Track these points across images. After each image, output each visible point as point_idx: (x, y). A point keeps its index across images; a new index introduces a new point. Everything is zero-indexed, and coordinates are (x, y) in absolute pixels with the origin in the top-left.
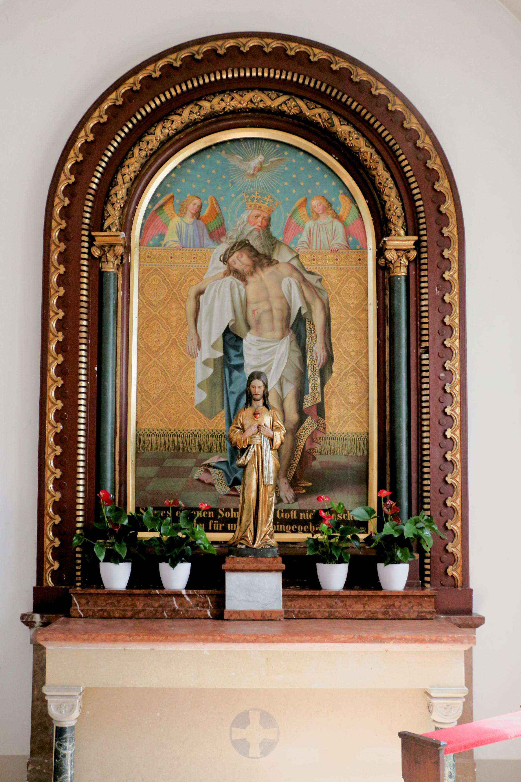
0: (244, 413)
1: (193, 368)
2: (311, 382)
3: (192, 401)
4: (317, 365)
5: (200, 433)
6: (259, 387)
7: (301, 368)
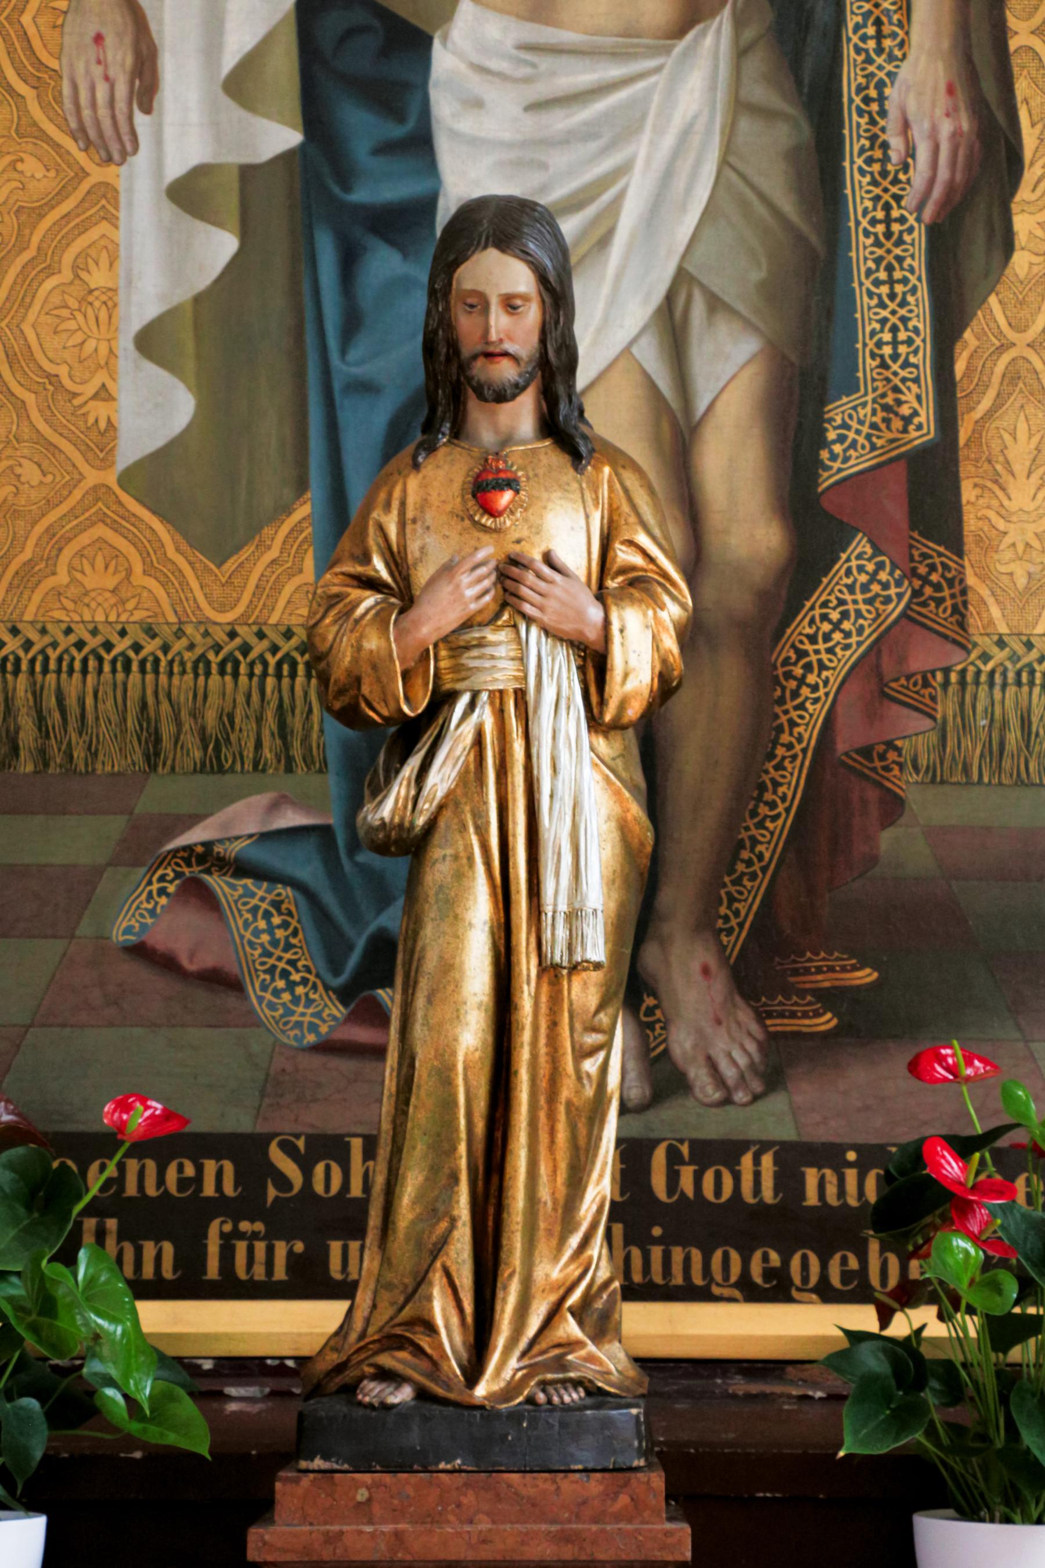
0: (413, 483)
1: (104, 227)
2: (868, 314)
3: (102, 441)
4: (910, 200)
5: (151, 647)
6: (510, 304)
7: (805, 228)
